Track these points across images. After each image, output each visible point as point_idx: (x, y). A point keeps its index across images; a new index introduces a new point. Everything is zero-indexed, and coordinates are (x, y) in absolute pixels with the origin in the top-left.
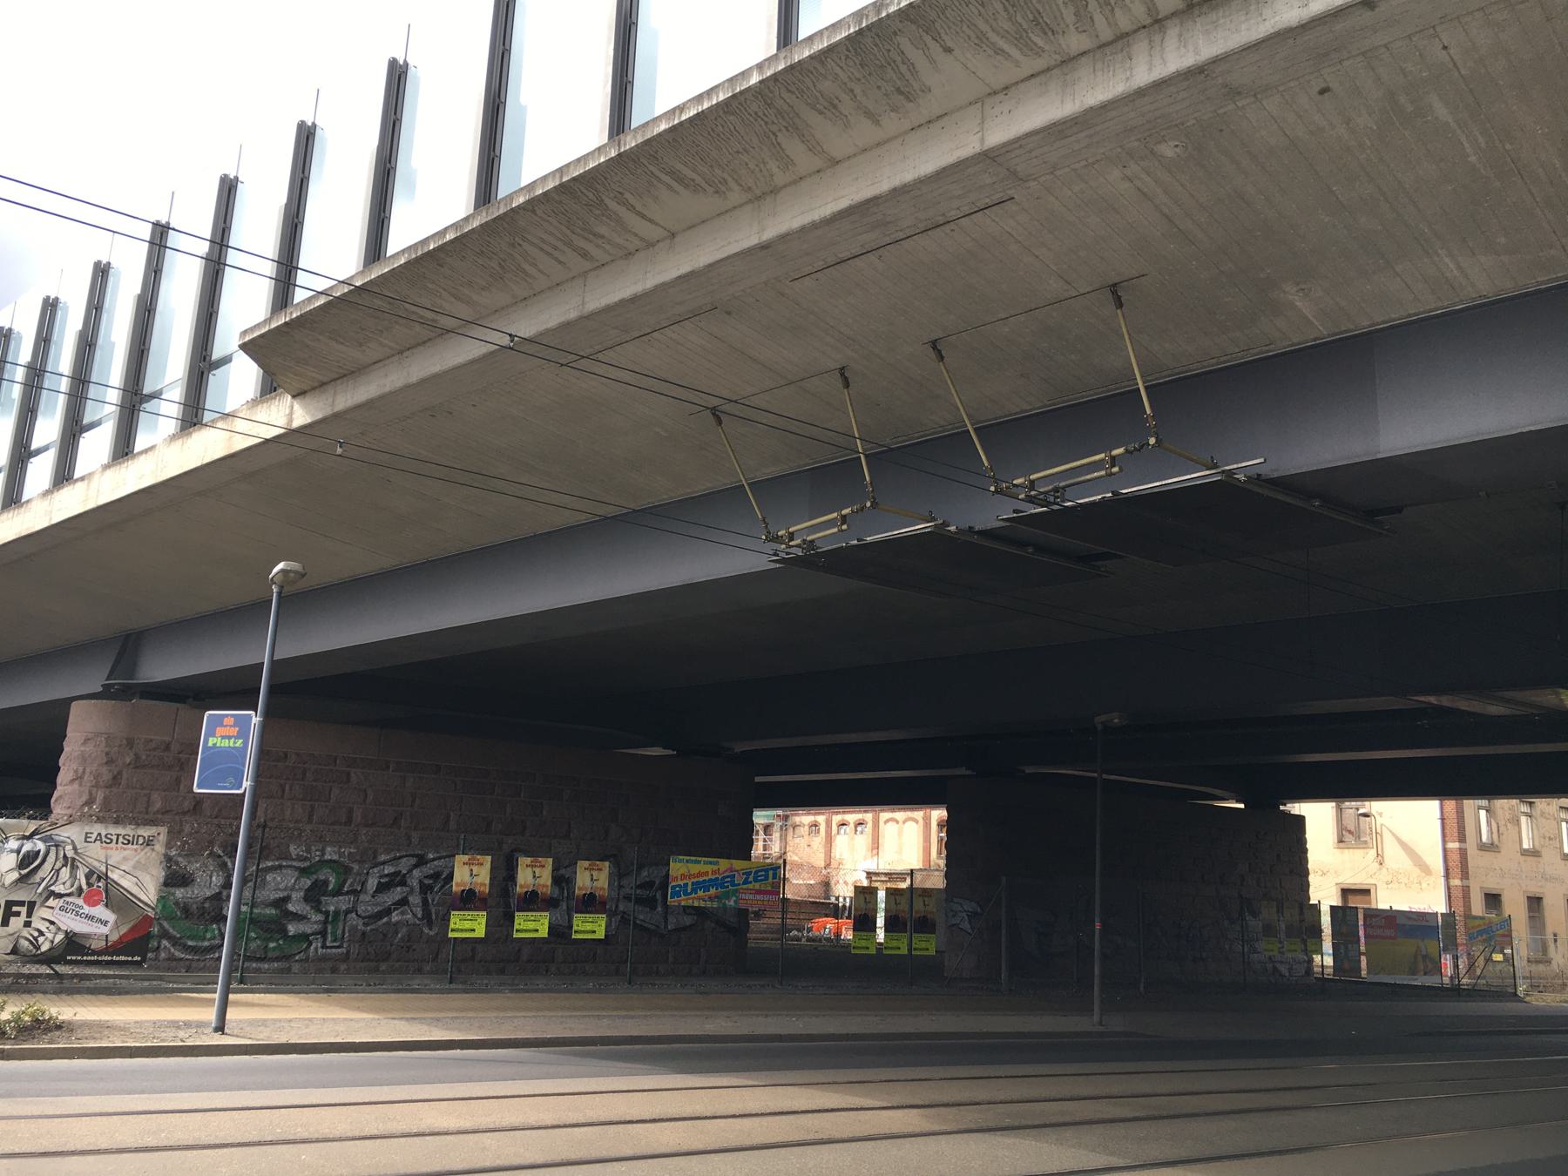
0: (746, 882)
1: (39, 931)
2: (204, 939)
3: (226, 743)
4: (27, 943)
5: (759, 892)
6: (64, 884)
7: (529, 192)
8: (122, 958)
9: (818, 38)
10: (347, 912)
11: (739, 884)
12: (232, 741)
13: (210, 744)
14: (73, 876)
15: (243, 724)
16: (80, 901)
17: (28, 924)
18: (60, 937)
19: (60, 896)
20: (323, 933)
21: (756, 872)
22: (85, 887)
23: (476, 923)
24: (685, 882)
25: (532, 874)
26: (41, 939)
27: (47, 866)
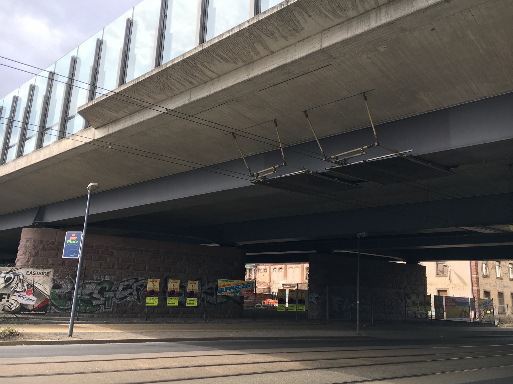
0: (243, 287)
1: (11, 303)
2: (66, 306)
3: (73, 242)
4: (7, 307)
5: (247, 291)
6: (20, 288)
7: (173, 62)
8: (39, 312)
9: (267, 12)
10: (113, 297)
11: (241, 288)
12: (75, 241)
13: (68, 242)
14: (23, 285)
15: (78, 236)
16: (25, 294)
17: (8, 301)
18: (18, 305)
19: (18, 292)
20: (105, 304)
21: (246, 284)
22: (26, 289)
23: (175, 301)
24: (223, 287)
25: (173, 285)
26: (12, 306)
27: (14, 282)
